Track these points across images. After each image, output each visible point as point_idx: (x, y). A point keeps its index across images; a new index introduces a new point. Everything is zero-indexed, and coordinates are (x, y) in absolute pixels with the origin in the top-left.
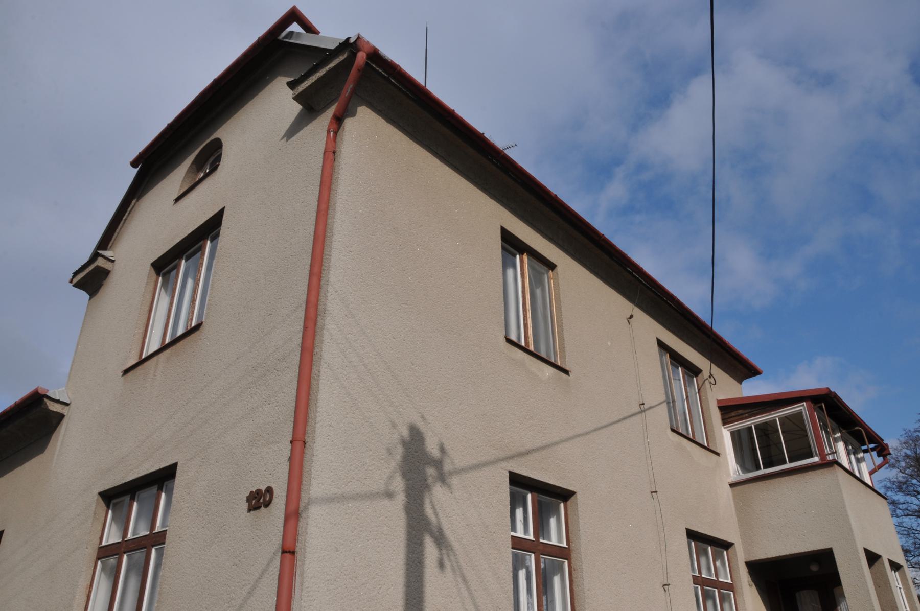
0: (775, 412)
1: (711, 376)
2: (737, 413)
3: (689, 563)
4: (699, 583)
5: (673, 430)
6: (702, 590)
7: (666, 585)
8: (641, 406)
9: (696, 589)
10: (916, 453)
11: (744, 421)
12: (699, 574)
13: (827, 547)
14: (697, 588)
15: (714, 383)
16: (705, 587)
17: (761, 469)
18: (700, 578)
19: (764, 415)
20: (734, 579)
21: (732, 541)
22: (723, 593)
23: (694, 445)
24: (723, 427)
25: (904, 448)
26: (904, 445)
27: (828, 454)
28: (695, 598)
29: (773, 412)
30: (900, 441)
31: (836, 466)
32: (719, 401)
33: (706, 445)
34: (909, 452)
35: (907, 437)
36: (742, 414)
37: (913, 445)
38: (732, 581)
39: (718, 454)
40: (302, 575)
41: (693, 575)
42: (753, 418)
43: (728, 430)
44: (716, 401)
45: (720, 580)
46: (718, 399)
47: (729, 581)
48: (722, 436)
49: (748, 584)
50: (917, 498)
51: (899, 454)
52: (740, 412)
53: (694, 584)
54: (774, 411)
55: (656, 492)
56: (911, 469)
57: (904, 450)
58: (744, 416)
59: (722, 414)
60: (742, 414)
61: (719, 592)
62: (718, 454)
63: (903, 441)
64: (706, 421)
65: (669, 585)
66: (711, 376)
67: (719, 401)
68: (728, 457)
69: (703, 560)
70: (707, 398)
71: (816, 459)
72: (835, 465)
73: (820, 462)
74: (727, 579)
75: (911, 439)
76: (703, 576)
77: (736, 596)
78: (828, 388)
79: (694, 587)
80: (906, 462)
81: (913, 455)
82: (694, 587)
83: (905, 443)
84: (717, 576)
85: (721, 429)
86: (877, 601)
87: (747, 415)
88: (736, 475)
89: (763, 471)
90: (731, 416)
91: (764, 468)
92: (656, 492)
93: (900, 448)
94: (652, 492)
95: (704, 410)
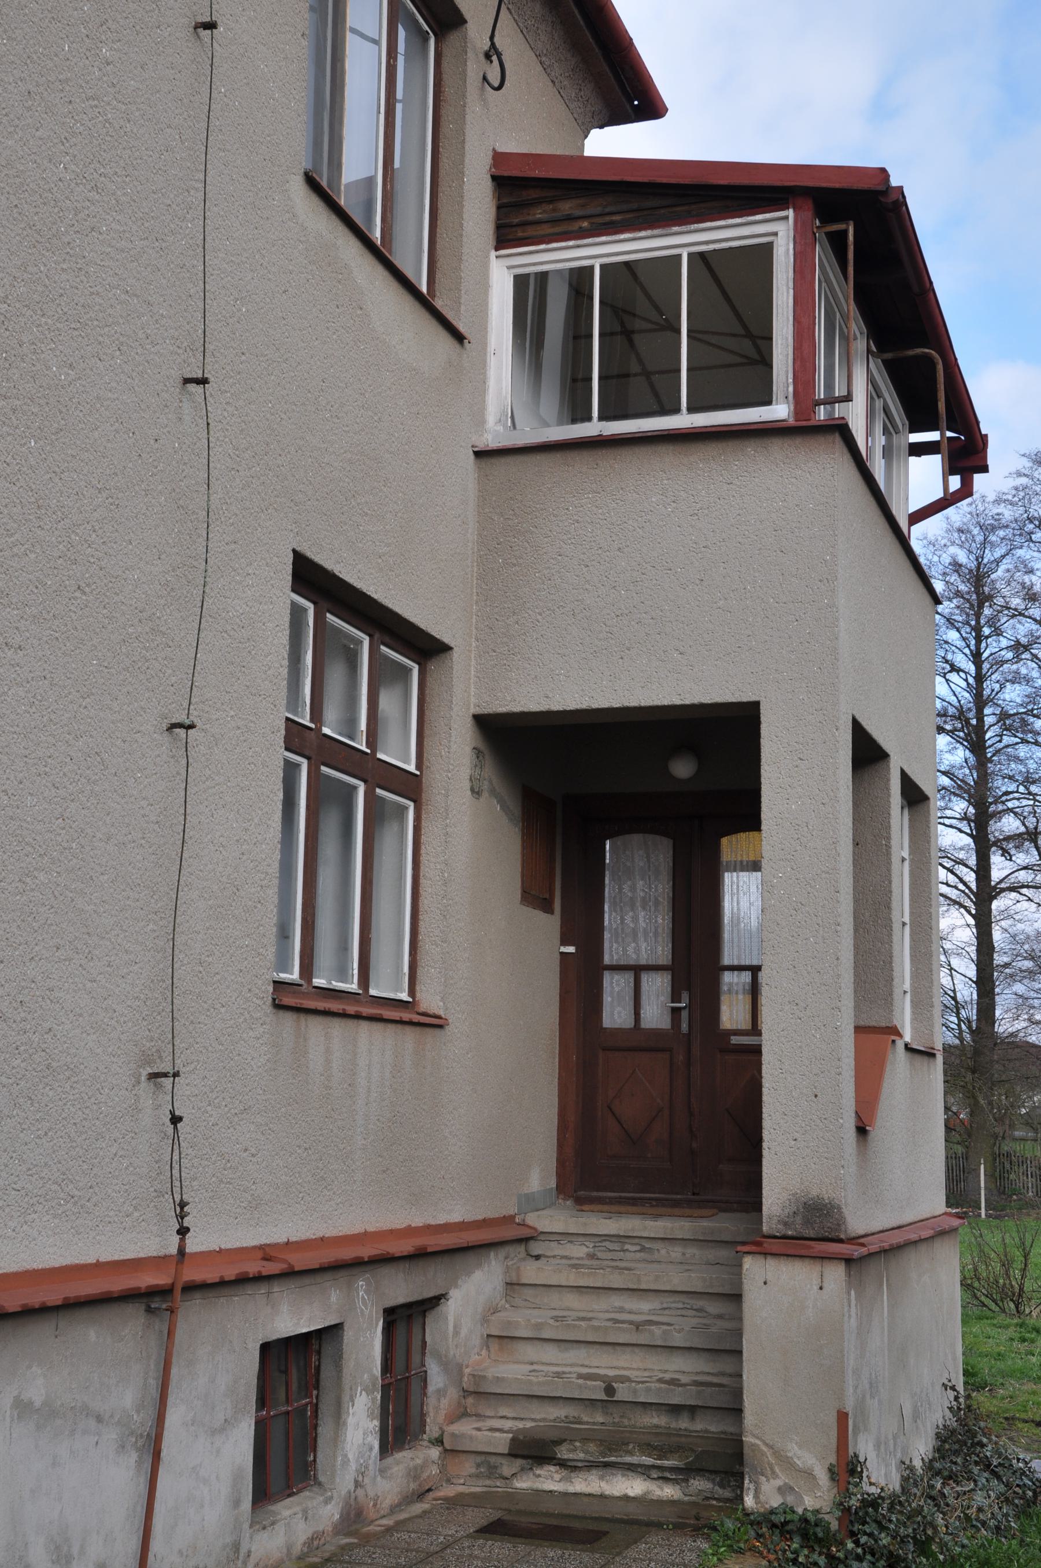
0: (683, 228)
1: (492, 53)
2: (554, 210)
3: (285, 672)
4: (307, 753)
5: (312, 182)
6: (314, 776)
7: (180, 725)
8: (201, 30)
9: (290, 771)
10: (979, 559)
11: (571, 243)
12: (312, 720)
13: (745, 698)
14: (298, 766)
15: (496, 84)
16: (323, 768)
17: (589, 419)
18: (313, 733)
19: (643, 234)
20: (426, 763)
21: (446, 639)
22: (382, 799)
23: (380, 272)
24: (493, 254)
25: (953, 543)
26: (956, 535)
27: (819, 403)
28: (281, 795)
29: (676, 229)
30: (948, 524)
31: (837, 438)
32: (498, 158)
33: (424, 289)
34: (963, 557)
35: (970, 513)
36: (570, 218)
37: (980, 538)
38: (419, 766)
39: (459, 337)
40: (157, 1388)
41: (288, 719)
42: (603, 239)
43: (509, 268)
44: (490, 154)
45: (380, 756)
46: (500, 150)
47: (412, 768)
48: (484, 285)
49: (467, 785)
50: (947, 680)
51: (936, 559)
52: (566, 207)
53: (287, 749)
54: (680, 225)
55: (203, 381)
56: (955, 601)
57: (953, 550)
58: (575, 226)
59: (499, 208)
60: (570, 218)
61: (369, 796)
62: (459, 337)
63: (957, 525)
64: (442, 215)
65: (191, 727)
66: (492, 53)
67: (498, 158)
68: (492, 362)
69: (335, 677)
70: (461, 132)
71: (780, 411)
72: (837, 435)
73: (792, 421)
74: (407, 761)
75: (978, 523)
76: (326, 730)
77: (424, 816)
78: (883, 171)
79: (294, 605)
80: (947, 582)
81: (973, 565)
82: (294, 605)
83: (960, 531)
84: (372, 742)
85: (488, 257)
86: (851, 876)
87: (585, 224)
88: (505, 426)
89: (594, 428)
90: (530, 218)
91: (601, 418)
92: (203, 381)
93: (943, 542)
94: (187, 381)
95: (442, 173)
